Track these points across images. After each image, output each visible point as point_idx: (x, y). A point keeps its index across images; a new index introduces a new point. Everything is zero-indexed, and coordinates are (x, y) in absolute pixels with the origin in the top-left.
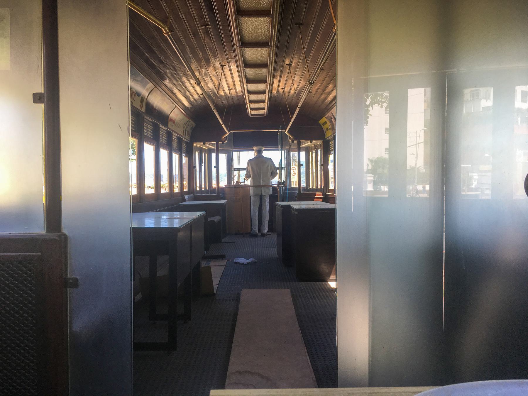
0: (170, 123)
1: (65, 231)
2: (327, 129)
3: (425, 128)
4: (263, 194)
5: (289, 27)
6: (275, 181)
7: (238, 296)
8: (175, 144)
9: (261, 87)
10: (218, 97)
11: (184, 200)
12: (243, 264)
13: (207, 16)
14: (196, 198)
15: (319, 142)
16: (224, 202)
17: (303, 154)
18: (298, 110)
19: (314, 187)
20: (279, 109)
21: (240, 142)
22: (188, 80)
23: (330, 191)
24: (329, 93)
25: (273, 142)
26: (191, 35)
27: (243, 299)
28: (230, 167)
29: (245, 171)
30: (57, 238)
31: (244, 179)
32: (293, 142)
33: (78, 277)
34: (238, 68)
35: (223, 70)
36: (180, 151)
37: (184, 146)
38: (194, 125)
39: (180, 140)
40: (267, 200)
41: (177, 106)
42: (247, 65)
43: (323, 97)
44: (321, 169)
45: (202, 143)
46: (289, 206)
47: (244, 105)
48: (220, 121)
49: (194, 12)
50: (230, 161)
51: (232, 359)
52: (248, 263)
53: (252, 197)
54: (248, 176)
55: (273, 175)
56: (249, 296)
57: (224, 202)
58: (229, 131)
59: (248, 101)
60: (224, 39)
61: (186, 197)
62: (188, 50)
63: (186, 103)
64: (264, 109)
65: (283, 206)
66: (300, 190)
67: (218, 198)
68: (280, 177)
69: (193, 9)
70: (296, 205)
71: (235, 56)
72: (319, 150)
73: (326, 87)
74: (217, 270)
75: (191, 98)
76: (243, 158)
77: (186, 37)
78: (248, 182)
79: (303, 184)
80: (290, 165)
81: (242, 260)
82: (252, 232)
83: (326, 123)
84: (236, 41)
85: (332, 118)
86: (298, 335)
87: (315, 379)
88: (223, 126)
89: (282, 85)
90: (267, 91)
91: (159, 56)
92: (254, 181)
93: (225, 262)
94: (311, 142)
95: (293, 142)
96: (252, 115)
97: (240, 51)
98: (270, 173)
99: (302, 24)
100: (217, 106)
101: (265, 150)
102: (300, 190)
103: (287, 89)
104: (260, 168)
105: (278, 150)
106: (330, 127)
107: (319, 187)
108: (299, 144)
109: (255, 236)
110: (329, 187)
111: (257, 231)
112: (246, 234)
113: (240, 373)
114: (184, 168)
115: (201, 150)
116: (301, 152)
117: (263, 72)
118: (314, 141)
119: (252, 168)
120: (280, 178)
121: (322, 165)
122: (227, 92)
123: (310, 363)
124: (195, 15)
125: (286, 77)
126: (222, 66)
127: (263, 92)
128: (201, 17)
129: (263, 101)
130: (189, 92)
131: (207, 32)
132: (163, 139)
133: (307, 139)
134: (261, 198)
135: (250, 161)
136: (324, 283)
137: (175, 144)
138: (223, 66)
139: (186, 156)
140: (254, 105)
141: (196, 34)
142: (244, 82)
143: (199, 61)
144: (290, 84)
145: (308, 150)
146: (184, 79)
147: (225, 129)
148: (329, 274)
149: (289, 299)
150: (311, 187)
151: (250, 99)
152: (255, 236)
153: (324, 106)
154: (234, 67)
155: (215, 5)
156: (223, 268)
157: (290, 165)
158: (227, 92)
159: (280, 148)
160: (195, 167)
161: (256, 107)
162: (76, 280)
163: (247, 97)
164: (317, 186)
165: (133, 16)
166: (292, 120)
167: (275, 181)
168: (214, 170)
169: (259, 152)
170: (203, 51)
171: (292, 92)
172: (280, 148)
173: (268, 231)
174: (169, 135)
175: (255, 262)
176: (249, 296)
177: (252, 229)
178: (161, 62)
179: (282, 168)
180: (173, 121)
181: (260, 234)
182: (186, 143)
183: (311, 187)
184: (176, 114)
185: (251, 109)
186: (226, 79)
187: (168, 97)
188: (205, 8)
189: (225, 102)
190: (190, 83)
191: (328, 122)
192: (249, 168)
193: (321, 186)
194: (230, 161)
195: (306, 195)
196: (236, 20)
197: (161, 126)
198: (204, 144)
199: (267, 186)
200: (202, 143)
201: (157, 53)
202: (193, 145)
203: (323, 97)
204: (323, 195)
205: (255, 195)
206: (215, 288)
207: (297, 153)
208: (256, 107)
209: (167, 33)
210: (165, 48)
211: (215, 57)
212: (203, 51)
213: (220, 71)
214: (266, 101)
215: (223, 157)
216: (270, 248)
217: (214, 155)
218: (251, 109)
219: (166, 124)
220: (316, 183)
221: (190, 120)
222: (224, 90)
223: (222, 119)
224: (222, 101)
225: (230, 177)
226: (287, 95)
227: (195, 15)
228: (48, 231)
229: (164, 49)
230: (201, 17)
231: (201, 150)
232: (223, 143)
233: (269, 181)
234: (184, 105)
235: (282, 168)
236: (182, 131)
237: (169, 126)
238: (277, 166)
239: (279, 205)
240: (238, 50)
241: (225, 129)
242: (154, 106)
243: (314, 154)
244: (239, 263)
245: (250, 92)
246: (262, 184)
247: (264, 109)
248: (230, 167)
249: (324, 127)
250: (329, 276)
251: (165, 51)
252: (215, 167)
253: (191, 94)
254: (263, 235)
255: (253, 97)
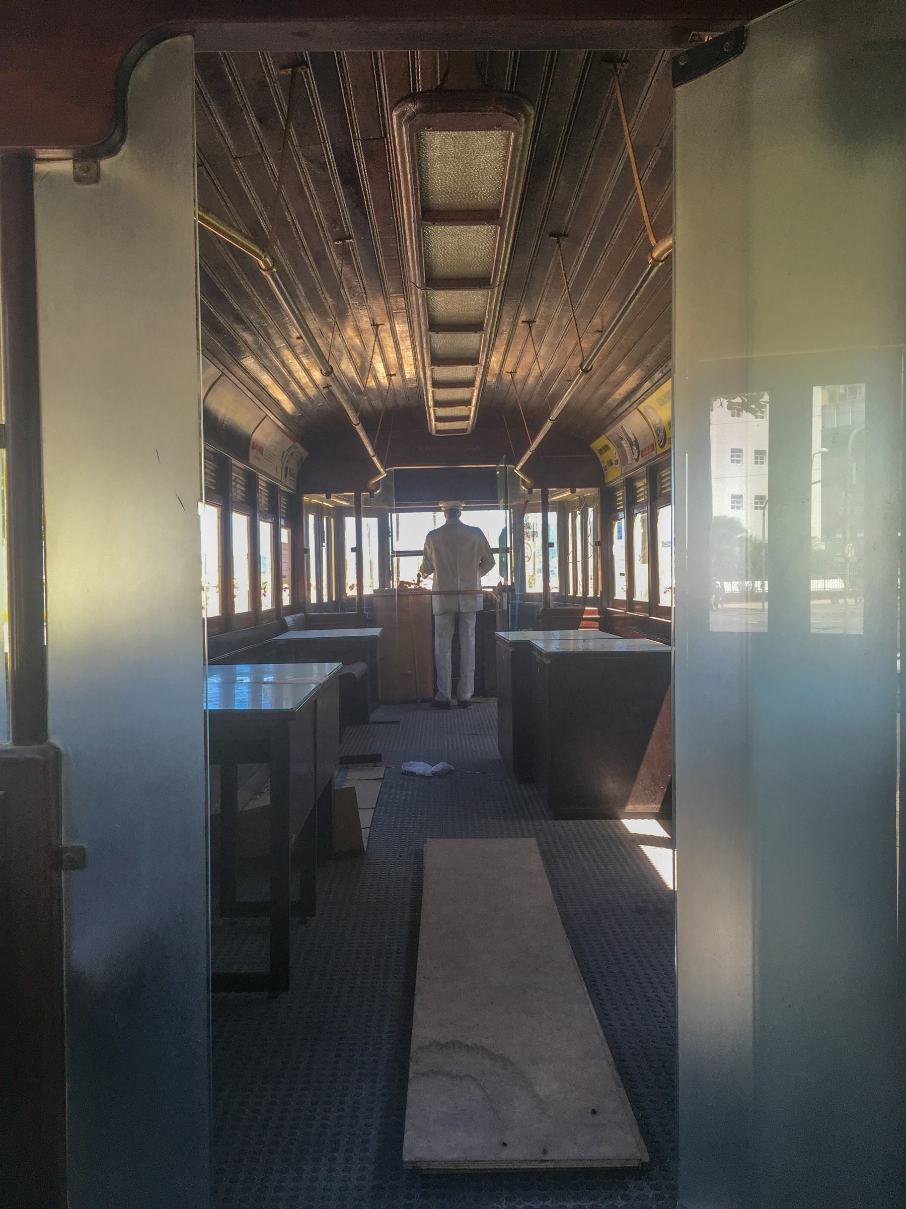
0: (252, 453)
1: (55, 740)
2: (610, 463)
3: (825, 450)
4: (463, 610)
5: (535, 239)
6: (491, 579)
7: (419, 856)
8: (263, 499)
9: (463, 372)
10: (359, 392)
11: (284, 628)
12: (422, 776)
13: (349, 221)
14: (309, 623)
15: (590, 492)
16: (375, 632)
17: (553, 517)
18: (549, 424)
19: (580, 595)
20: (503, 421)
21: (410, 493)
22: (296, 357)
23: (619, 603)
24: (619, 384)
25: (485, 493)
26: (309, 260)
27: (429, 863)
28: (388, 549)
29: (422, 558)
30: (38, 756)
31: (419, 576)
32: (530, 492)
33: (86, 845)
34: (411, 329)
35: (377, 335)
36: (273, 514)
37: (282, 501)
38: (305, 454)
39: (272, 489)
40: (472, 623)
41: (269, 414)
42: (435, 326)
43: (602, 391)
44: (595, 551)
45: (324, 496)
46: (528, 646)
47: (421, 408)
48: (369, 449)
49: (319, 212)
50: (385, 534)
51: (419, 1013)
52: (434, 774)
53: (437, 618)
54: (425, 570)
55: (486, 566)
56: (444, 856)
57: (375, 632)
58: (384, 469)
59: (431, 403)
60: (383, 266)
61: (289, 619)
62: (301, 291)
63: (288, 406)
64: (466, 418)
65: (514, 644)
66: (547, 603)
67: (361, 621)
68: (503, 572)
69: (318, 204)
70: (550, 642)
71: (407, 305)
72: (590, 510)
73: (612, 370)
74: (365, 787)
75: (301, 395)
76: (415, 527)
77: (297, 264)
78: (428, 584)
79: (555, 584)
80: (529, 547)
81: (420, 767)
82: (437, 698)
83: (606, 448)
84: (414, 274)
85: (621, 439)
86: (564, 954)
87: (611, 1060)
88: (375, 459)
89: (509, 366)
90: (478, 380)
91: (236, 306)
92: (439, 581)
93: (380, 772)
94: (573, 492)
95: (530, 492)
96: (438, 431)
97: (423, 296)
98: (477, 562)
99: (565, 235)
100: (368, 420)
101: (465, 509)
102: (547, 603)
103: (520, 374)
104: (454, 551)
105: (497, 508)
106: (617, 457)
107: (591, 594)
108: (545, 496)
109: (445, 706)
110: (614, 595)
111: (449, 695)
112: (423, 701)
113: (442, 1047)
114: (283, 552)
115: (320, 511)
116: (550, 514)
117: (470, 341)
118: (578, 490)
119: (437, 551)
120: (501, 574)
121: (596, 544)
122: (384, 381)
123: (597, 1021)
124: (322, 216)
125: (520, 347)
126: (375, 326)
127: (469, 384)
128: (335, 220)
129: (467, 403)
130: (298, 383)
131: (345, 254)
132: (238, 491)
133: (562, 485)
134: (457, 619)
135: (432, 534)
136: (611, 821)
137: (263, 499)
138: (378, 326)
139: (286, 527)
140: (442, 412)
141: (320, 258)
142: (427, 361)
143: (322, 313)
144: (525, 359)
145: (563, 509)
146: (287, 355)
147: (378, 465)
148: (624, 801)
149: (535, 863)
150: (571, 593)
151: (438, 397)
152: (445, 706)
153: (603, 412)
154: (401, 328)
155: (369, 196)
156: (377, 786)
157: (529, 547)
158: (384, 381)
159: (501, 502)
160: (307, 551)
161: (452, 412)
162: (82, 852)
163: (430, 394)
164: (586, 591)
165: (206, 240)
166: (534, 446)
167: (491, 579)
168: (350, 559)
169: (453, 514)
170: (338, 297)
171: (531, 381)
172: (501, 502)
173: (474, 696)
174: (251, 479)
175: (451, 771)
176: (444, 856)
177: (436, 690)
178: (239, 320)
179: (506, 550)
180: (261, 450)
181: (454, 702)
182: (288, 496)
183: (571, 593)
184: (266, 433)
185: (438, 419)
186: (386, 352)
187: (249, 394)
188: (344, 203)
189: (377, 403)
190: (301, 363)
191: (611, 446)
192: (429, 551)
193: (596, 592)
194: (385, 534)
195: (560, 613)
196: (419, 231)
197: (235, 462)
198: (328, 497)
199: (473, 591)
200: (324, 496)
201: (232, 301)
202: (301, 500)
203: (602, 391)
204: (600, 612)
205: (444, 613)
206: (365, 833)
207: (540, 515)
208: (452, 412)
209: (268, 269)
210: (249, 289)
211: (362, 303)
212: (338, 297)
213: (370, 337)
214: (474, 403)
215: (371, 524)
216: (482, 734)
217: (350, 522)
218: (438, 419)
219: (244, 456)
220: (584, 584)
221: (297, 444)
222: (375, 378)
223: (372, 442)
224: (370, 400)
225: (386, 572)
226: (519, 386)
227: (322, 216)
228: (17, 740)
229: (248, 290)
230: (335, 220)
231: (320, 511)
232: (372, 496)
233: (475, 581)
234: (282, 409)
235: (506, 550)
236: (279, 470)
237: (252, 460)
238: (494, 543)
239: (504, 641)
240: (416, 295)
241: (378, 465)
242: (220, 417)
243: (579, 517)
244: (412, 774)
245: (436, 384)
246: (461, 587)
247: (466, 418)
248: (388, 549)
249: (603, 458)
250: (624, 806)
251: (248, 296)
252: (353, 550)
253: (301, 388)
254: (463, 704)
255: (445, 394)
